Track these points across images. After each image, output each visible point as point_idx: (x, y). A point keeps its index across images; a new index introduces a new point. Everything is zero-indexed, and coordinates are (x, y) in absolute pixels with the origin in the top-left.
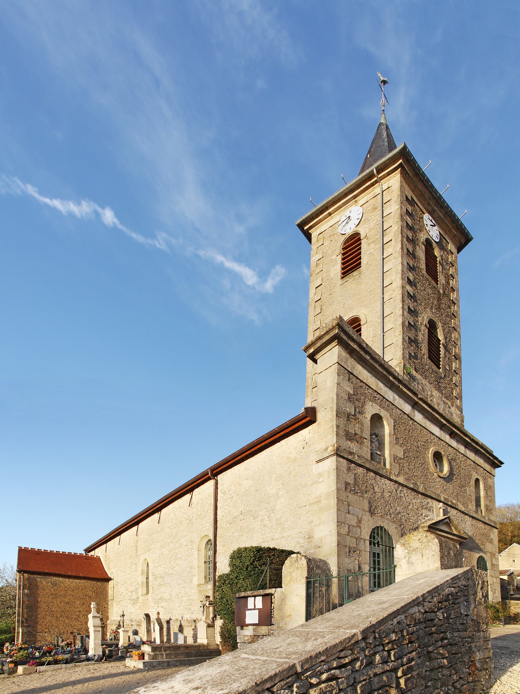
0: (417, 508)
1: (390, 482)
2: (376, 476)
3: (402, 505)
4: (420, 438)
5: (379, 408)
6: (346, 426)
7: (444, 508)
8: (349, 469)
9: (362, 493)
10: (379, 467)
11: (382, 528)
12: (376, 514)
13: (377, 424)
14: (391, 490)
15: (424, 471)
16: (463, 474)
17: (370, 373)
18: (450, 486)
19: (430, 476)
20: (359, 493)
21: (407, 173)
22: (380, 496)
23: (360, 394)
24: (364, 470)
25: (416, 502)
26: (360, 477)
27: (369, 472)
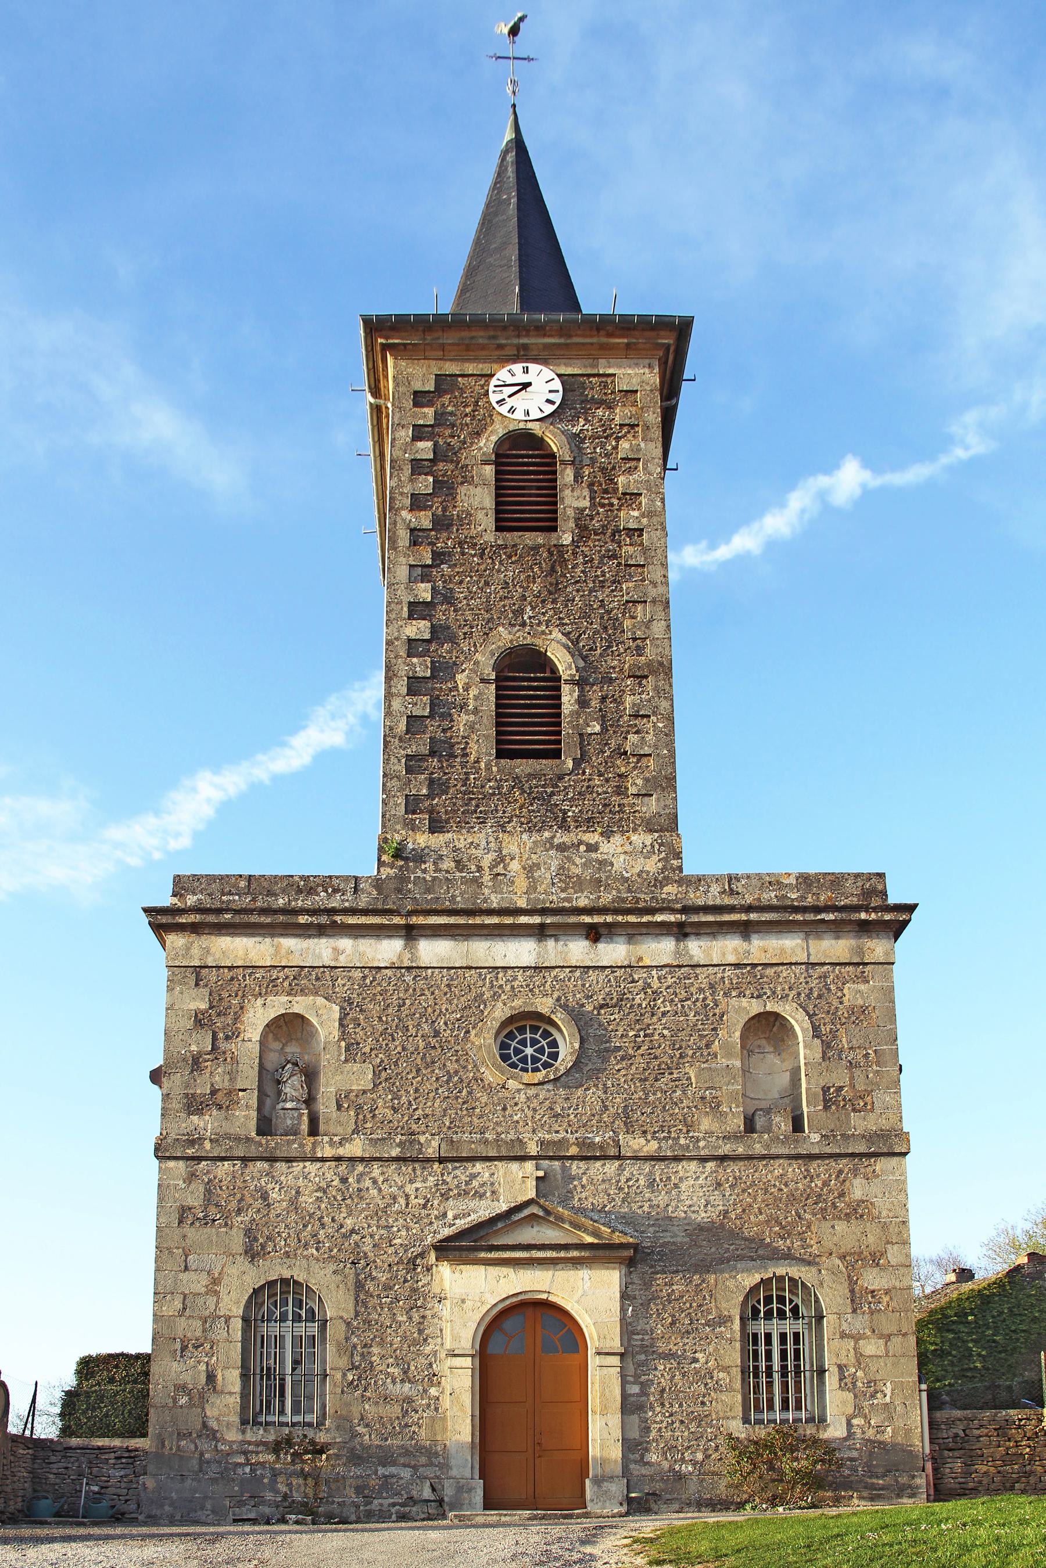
0: (422, 1202)
1: (319, 1165)
3: (364, 1210)
5: (287, 998)
7: (541, 1174)
8: (192, 1177)
11: (285, 1282)
12: (270, 1252)
14: (323, 1184)
16: (665, 1032)
19: (484, 1099)
21: (405, 345)
23: (230, 996)
24: (234, 1165)
25: (417, 1189)
26: (222, 1184)
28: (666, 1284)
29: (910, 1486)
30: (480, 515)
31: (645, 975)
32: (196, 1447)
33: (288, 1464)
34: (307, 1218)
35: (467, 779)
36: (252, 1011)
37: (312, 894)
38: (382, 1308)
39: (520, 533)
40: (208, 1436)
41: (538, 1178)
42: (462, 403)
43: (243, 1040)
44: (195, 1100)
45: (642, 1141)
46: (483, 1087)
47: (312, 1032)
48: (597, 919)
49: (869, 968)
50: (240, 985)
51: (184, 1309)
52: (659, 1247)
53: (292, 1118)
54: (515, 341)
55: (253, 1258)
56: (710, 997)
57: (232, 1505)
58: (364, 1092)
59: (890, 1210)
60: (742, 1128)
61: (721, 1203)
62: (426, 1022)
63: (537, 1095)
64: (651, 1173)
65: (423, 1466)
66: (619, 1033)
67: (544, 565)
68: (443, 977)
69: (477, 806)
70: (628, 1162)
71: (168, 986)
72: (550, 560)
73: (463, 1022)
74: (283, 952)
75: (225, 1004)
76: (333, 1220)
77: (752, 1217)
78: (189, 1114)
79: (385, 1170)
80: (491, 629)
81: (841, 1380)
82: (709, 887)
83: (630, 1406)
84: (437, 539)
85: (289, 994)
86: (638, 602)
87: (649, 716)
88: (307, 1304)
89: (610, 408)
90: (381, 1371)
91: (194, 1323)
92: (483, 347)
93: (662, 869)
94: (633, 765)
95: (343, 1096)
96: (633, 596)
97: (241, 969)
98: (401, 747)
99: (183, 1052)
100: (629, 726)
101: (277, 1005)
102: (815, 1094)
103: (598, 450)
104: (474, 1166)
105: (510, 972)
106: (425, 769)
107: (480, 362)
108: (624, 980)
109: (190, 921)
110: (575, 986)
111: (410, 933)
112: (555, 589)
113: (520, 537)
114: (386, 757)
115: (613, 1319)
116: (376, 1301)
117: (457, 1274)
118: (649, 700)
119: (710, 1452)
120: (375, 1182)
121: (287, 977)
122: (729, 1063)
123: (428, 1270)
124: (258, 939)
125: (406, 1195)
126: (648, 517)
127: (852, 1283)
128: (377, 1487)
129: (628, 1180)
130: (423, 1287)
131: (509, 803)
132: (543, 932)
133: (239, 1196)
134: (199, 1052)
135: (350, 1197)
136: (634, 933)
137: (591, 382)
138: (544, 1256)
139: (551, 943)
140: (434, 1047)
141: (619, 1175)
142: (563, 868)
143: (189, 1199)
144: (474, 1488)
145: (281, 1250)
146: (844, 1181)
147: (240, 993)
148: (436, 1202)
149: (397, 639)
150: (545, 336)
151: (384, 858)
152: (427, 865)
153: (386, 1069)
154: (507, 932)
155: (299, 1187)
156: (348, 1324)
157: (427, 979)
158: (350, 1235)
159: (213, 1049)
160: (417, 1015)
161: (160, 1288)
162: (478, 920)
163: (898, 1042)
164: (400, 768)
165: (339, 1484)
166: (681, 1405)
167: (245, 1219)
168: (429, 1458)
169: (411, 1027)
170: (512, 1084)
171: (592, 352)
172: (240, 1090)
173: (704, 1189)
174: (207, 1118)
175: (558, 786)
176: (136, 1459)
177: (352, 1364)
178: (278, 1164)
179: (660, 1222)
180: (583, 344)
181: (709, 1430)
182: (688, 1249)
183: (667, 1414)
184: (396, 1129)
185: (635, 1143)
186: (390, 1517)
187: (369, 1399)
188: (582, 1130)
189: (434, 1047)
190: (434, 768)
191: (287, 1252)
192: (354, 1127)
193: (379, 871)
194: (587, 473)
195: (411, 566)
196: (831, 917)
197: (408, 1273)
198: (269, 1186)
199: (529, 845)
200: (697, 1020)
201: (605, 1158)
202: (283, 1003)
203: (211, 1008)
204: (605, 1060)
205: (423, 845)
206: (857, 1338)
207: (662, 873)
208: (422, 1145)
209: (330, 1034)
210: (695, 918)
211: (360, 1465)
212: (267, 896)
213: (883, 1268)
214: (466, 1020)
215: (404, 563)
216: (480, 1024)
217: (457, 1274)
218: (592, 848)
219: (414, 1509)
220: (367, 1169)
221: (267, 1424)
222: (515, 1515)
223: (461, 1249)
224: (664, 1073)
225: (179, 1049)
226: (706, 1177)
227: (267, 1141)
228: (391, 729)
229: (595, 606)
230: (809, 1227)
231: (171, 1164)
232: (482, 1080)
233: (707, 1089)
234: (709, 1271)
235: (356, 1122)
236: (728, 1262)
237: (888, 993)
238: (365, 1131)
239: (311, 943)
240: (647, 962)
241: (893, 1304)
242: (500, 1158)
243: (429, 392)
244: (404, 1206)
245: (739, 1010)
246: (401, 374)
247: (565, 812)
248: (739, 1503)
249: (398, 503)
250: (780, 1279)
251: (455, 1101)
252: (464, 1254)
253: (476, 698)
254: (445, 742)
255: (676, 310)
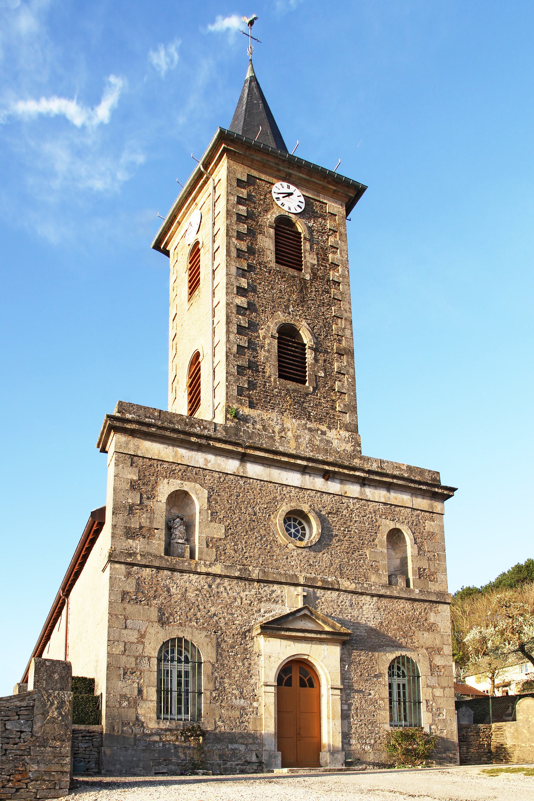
0: (249, 602)
1: (197, 576)
2: (172, 574)
3: (220, 603)
4: (259, 500)
5: (180, 481)
6: (126, 523)
7: (305, 594)
8: (128, 575)
9: (148, 600)
10: (176, 561)
11: (180, 640)
12: (171, 622)
13: (186, 501)
14: (199, 587)
15: (266, 546)
16: (356, 531)
17: (164, 444)
18: (325, 557)
19: (278, 552)
20: (143, 601)
21: (235, 152)
22: (179, 599)
23: (150, 475)
24: (152, 571)
25: (246, 595)
26: (145, 581)
27: (161, 571)
28: (358, 656)
29: (454, 758)
30: (269, 252)
31: (347, 501)
32: (132, 731)
33: (183, 742)
34: (191, 605)
35: (265, 385)
36: (162, 485)
37: (193, 427)
38: (230, 658)
39: (287, 268)
40: (139, 725)
41: (304, 596)
42: (259, 193)
43: (157, 501)
44: (130, 530)
45: (349, 583)
46: (277, 545)
47: (188, 503)
48: (331, 468)
49: (434, 515)
50: (155, 469)
51: (125, 651)
52: (355, 636)
53: (182, 549)
54: (287, 170)
55: (163, 625)
56: (374, 517)
57: (154, 765)
58: (220, 539)
59: (444, 629)
60: (387, 582)
61: (380, 618)
62: (250, 507)
63: (302, 553)
64: (351, 600)
65: (250, 744)
66: (337, 528)
67: (298, 287)
68: (258, 484)
69: (270, 400)
70: (342, 593)
71: (115, 463)
72: (301, 285)
73: (268, 510)
74: (179, 455)
75: (147, 479)
76: (205, 608)
77: (392, 626)
78: (128, 538)
79: (231, 583)
80: (275, 312)
81: (427, 707)
82: (373, 463)
83: (345, 716)
84: (249, 258)
85: (182, 480)
86: (339, 318)
87: (344, 375)
88: (184, 653)
89: (325, 219)
90: (229, 692)
91: (131, 659)
92: (271, 168)
93: (353, 450)
94: (338, 396)
95: (209, 540)
96: (337, 314)
97: (156, 461)
98: (234, 360)
99: (124, 502)
100: (336, 377)
101: (174, 485)
102: (416, 571)
103: (320, 238)
104: (273, 586)
105: (288, 488)
106: (245, 375)
107: (268, 176)
108: (338, 502)
109: (132, 428)
110: (317, 501)
111: (244, 458)
112: (303, 301)
113: (287, 269)
114: (228, 363)
115: (337, 671)
116: (226, 653)
117: (267, 642)
118: (345, 367)
119: (377, 739)
120: (225, 589)
121: (180, 470)
122: (382, 550)
123: (252, 639)
124: (166, 446)
125: (241, 598)
126: (342, 277)
127: (431, 662)
128: (230, 755)
129: (342, 602)
130: (249, 648)
131: (285, 402)
132: (305, 470)
133: (155, 588)
134: (133, 504)
135: (213, 596)
136: (344, 479)
137: (316, 204)
138: (311, 636)
139: (307, 477)
140: (254, 521)
141: (338, 599)
142: (311, 440)
143: (127, 587)
144: (277, 756)
145: (177, 621)
146: (427, 613)
147: (155, 474)
148: (256, 603)
149: (232, 303)
150: (300, 172)
151: (229, 416)
152: (249, 424)
153: (231, 529)
154: (288, 467)
155: (187, 587)
156: (213, 665)
157: (250, 484)
158: (213, 617)
159: (140, 503)
160: (246, 503)
161: (111, 638)
162: (278, 458)
163: (446, 551)
164: (234, 371)
165: (210, 753)
166: (365, 716)
167: (158, 602)
168: (254, 740)
169: (243, 508)
170: (291, 546)
171: (319, 189)
172: (155, 529)
173: (373, 610)
174: (137, 542)
175: (306, 399)
176: (94, 737)
177: (215, 687)
178: (175, 573)
179: (355, 624)
180: (316, 183)
181: (376, 729)
182: (367, 639)
183: (359, 720)
184: (236, 562)
185: (346, 584)
186: (236, 771)
187: (224, 707)
188: (321, 574)
189: (254, 521)
190: (250, 375)
191: (180, 623)
192: (215, 558)
193: (226, 423)
194: (315, 248)
195: (238, 268)
196: (424, 488)
197: (242, 640)
198: (171, 585)
199: (296, 425)
200: (369, 527)
201: (333, 589)
202: (179, 484)
203: (139, 480)
204: (331, 540)
205: (247, 414)
206: (433, 687)
207: (353, 452)
208: (250, 571)
209: (203, 505)
210: (372, 477)
211: (219, 743)
212: (170, 423)
213: (442, 656)
214: (269, 509)
215: (234, 265)
216: (276, 512)
217: (267, 642)
218: (324, 433)
219: (248, 767)
220: (222, 582)
221: (171, 719)
222: (317, 769)
223: (273, 629)
224: (356, 551)
225: (122, 500)
226: (374, 605)
227: (171, 560)
228: (230, 349)
229: (320, 314)
230: (414, 633)
231: (117, 566)
232: (277, 542)
233: (374, 561)
234: (375, 651)
235: (216, 555)
236: (383, 647)
237: (442, 527)
238: (221, 561)
239: (193, 454)
240: (348, 495)
241: (446, 673)
242: (286, 584)
243: (244, 181)
244: (240, 604)
245: (386, 525)
246: (231, 167)
247: (310, 413)
248: (390, 765)
249: (230, 233)
250: (403, 657)
251: (264, 551)
252: (274, 632)
253: (269, 344)
254: (254, 363)
255: (361, 180)
